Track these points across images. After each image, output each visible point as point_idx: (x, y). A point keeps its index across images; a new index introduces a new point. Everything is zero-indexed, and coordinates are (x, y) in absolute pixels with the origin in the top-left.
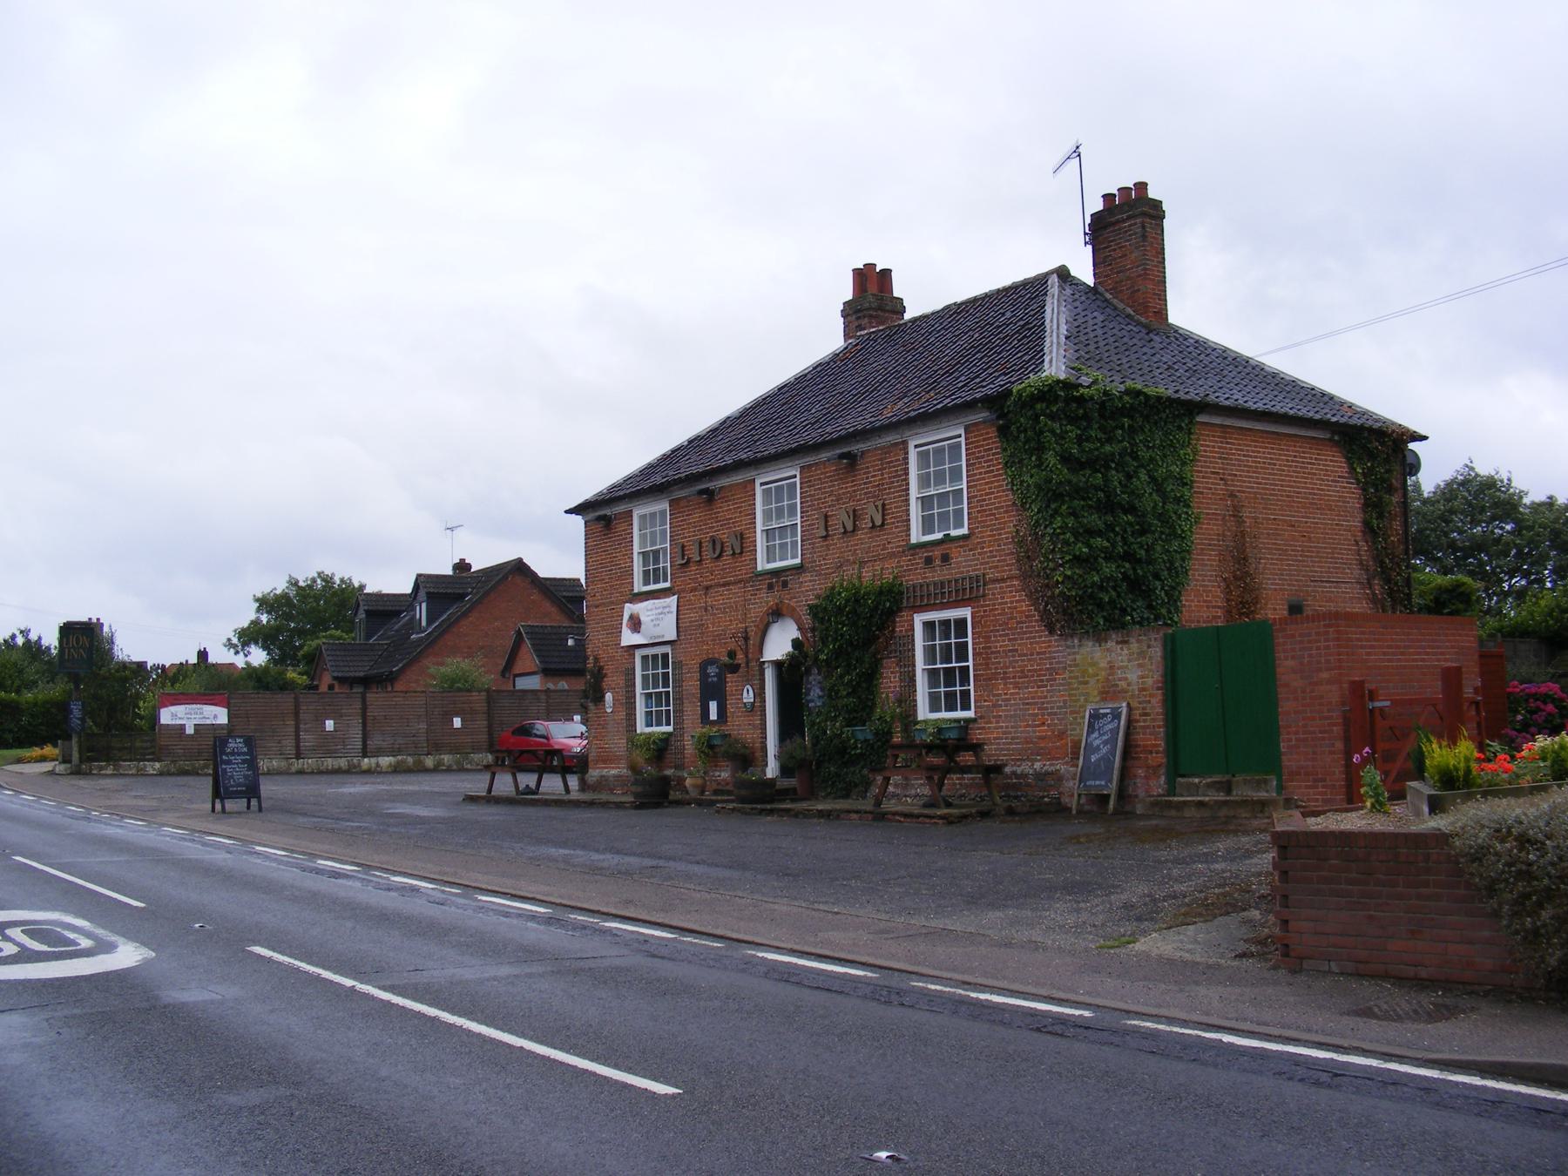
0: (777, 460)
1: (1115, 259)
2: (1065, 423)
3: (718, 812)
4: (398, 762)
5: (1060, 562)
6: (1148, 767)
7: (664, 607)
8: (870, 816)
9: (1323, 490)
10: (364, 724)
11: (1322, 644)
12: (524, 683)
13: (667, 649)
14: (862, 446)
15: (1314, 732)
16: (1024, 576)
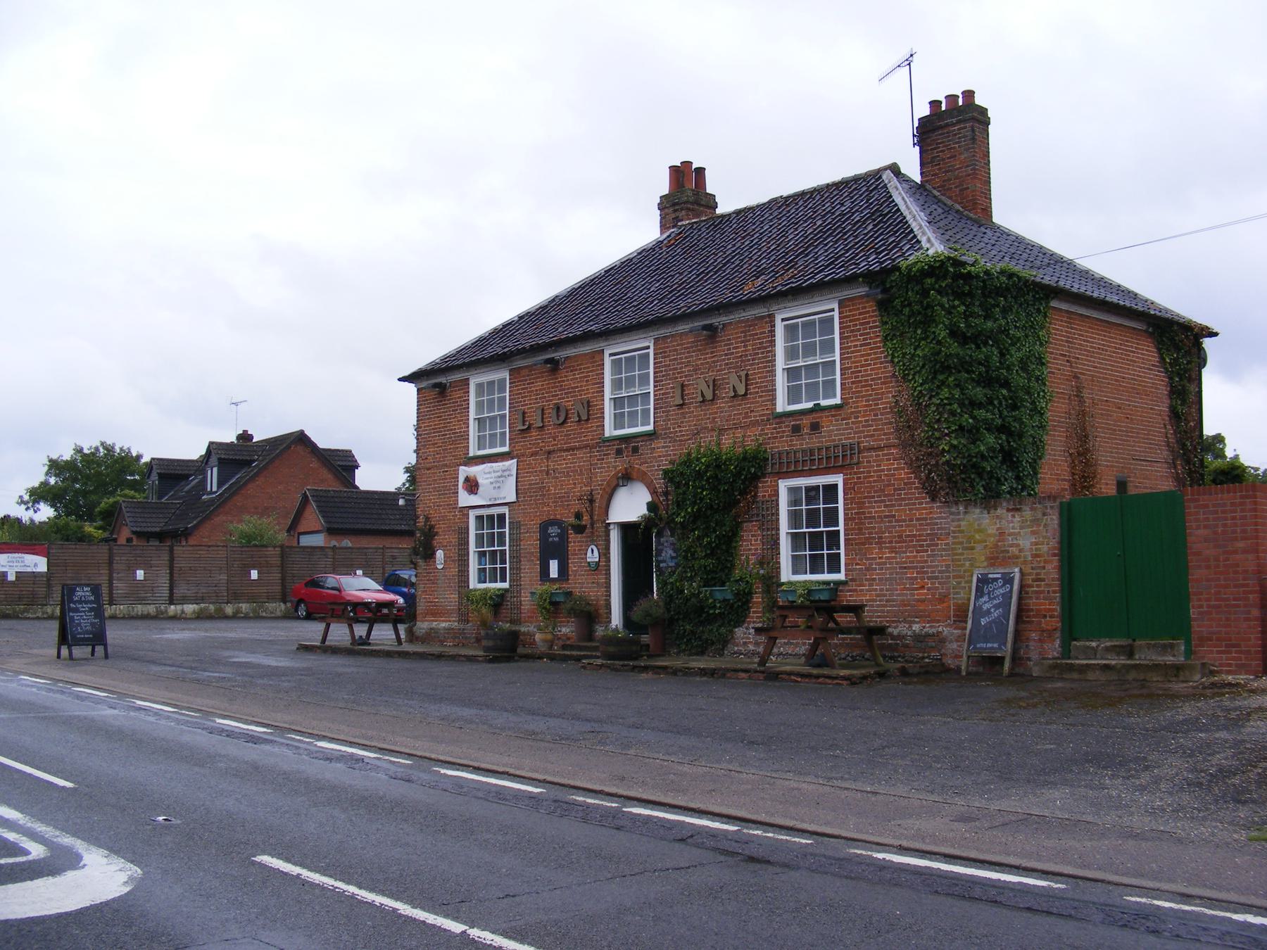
0: (622, 333)
1: (943, 160)
2: (951, 298)
3: (584, 667)
4: (201, 609)
5: (946, 431)
6: (1043, 631)
7: (504, 471)
8: (761, 676)
9: (1141, 376)
10: (171, 574)
11: (1238, 514)
12: (306, 541)
13: (505, 510)
14: (724, 318)
15: (1228, 600)
16: (904, 445)
